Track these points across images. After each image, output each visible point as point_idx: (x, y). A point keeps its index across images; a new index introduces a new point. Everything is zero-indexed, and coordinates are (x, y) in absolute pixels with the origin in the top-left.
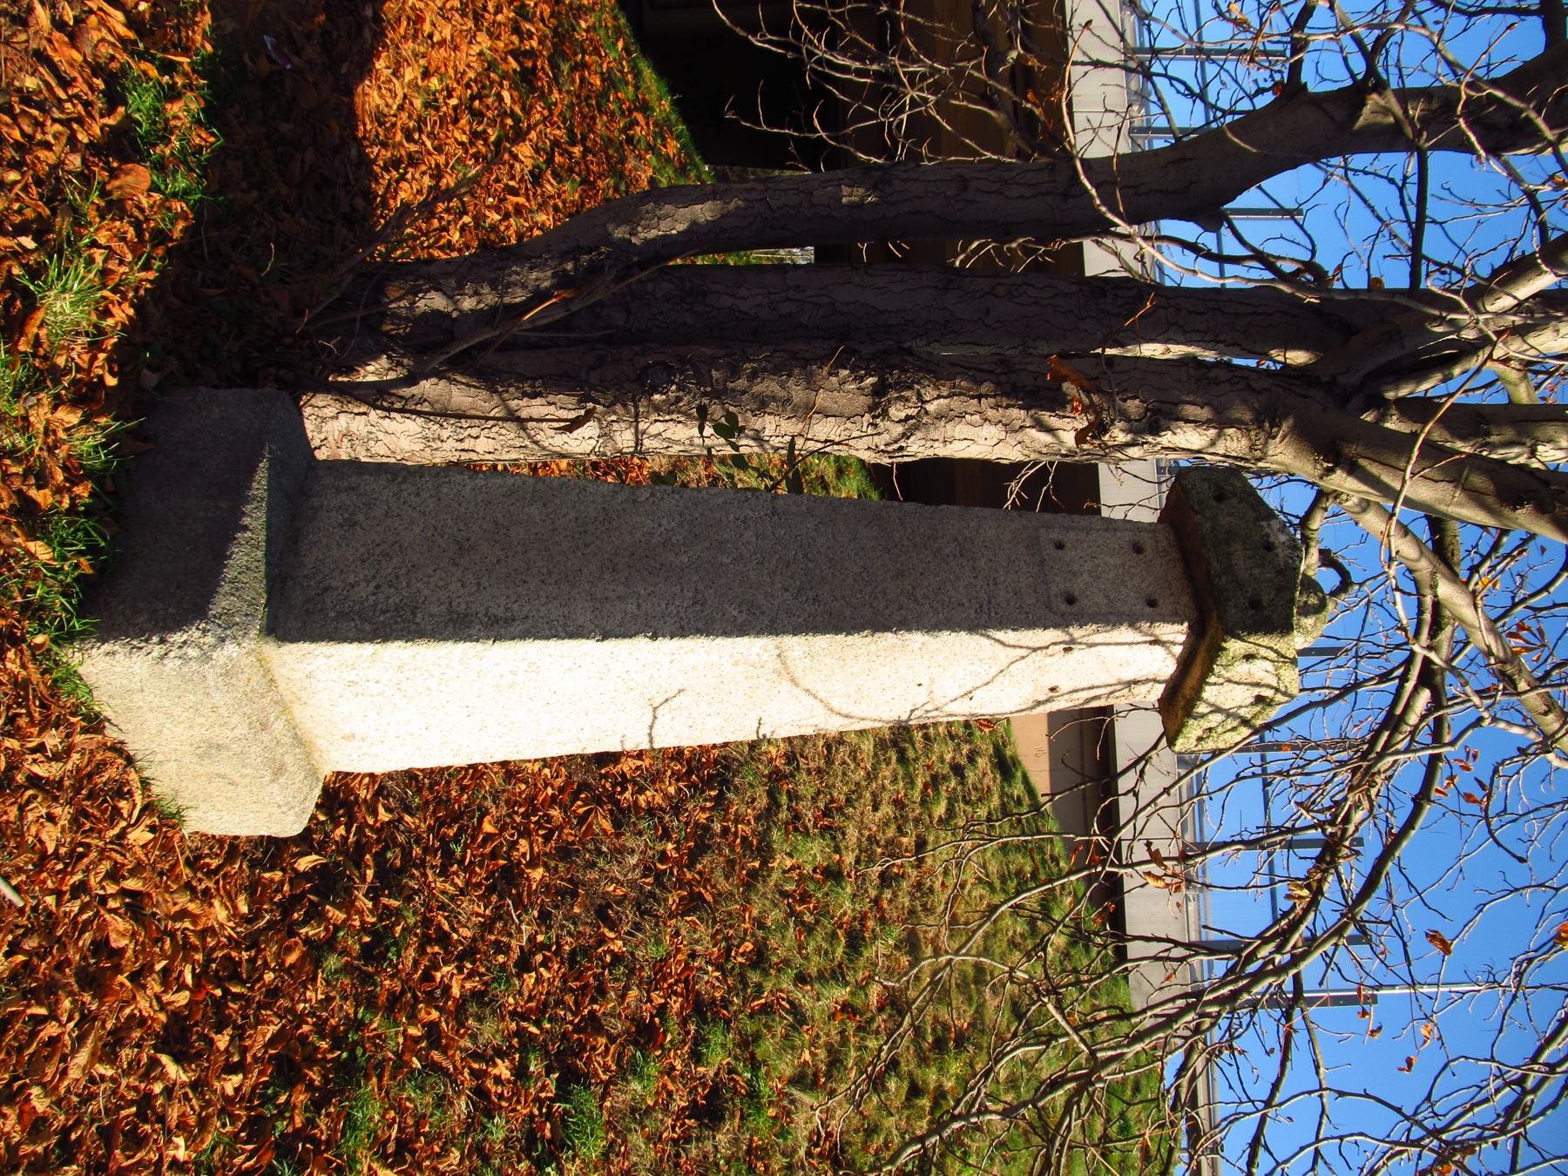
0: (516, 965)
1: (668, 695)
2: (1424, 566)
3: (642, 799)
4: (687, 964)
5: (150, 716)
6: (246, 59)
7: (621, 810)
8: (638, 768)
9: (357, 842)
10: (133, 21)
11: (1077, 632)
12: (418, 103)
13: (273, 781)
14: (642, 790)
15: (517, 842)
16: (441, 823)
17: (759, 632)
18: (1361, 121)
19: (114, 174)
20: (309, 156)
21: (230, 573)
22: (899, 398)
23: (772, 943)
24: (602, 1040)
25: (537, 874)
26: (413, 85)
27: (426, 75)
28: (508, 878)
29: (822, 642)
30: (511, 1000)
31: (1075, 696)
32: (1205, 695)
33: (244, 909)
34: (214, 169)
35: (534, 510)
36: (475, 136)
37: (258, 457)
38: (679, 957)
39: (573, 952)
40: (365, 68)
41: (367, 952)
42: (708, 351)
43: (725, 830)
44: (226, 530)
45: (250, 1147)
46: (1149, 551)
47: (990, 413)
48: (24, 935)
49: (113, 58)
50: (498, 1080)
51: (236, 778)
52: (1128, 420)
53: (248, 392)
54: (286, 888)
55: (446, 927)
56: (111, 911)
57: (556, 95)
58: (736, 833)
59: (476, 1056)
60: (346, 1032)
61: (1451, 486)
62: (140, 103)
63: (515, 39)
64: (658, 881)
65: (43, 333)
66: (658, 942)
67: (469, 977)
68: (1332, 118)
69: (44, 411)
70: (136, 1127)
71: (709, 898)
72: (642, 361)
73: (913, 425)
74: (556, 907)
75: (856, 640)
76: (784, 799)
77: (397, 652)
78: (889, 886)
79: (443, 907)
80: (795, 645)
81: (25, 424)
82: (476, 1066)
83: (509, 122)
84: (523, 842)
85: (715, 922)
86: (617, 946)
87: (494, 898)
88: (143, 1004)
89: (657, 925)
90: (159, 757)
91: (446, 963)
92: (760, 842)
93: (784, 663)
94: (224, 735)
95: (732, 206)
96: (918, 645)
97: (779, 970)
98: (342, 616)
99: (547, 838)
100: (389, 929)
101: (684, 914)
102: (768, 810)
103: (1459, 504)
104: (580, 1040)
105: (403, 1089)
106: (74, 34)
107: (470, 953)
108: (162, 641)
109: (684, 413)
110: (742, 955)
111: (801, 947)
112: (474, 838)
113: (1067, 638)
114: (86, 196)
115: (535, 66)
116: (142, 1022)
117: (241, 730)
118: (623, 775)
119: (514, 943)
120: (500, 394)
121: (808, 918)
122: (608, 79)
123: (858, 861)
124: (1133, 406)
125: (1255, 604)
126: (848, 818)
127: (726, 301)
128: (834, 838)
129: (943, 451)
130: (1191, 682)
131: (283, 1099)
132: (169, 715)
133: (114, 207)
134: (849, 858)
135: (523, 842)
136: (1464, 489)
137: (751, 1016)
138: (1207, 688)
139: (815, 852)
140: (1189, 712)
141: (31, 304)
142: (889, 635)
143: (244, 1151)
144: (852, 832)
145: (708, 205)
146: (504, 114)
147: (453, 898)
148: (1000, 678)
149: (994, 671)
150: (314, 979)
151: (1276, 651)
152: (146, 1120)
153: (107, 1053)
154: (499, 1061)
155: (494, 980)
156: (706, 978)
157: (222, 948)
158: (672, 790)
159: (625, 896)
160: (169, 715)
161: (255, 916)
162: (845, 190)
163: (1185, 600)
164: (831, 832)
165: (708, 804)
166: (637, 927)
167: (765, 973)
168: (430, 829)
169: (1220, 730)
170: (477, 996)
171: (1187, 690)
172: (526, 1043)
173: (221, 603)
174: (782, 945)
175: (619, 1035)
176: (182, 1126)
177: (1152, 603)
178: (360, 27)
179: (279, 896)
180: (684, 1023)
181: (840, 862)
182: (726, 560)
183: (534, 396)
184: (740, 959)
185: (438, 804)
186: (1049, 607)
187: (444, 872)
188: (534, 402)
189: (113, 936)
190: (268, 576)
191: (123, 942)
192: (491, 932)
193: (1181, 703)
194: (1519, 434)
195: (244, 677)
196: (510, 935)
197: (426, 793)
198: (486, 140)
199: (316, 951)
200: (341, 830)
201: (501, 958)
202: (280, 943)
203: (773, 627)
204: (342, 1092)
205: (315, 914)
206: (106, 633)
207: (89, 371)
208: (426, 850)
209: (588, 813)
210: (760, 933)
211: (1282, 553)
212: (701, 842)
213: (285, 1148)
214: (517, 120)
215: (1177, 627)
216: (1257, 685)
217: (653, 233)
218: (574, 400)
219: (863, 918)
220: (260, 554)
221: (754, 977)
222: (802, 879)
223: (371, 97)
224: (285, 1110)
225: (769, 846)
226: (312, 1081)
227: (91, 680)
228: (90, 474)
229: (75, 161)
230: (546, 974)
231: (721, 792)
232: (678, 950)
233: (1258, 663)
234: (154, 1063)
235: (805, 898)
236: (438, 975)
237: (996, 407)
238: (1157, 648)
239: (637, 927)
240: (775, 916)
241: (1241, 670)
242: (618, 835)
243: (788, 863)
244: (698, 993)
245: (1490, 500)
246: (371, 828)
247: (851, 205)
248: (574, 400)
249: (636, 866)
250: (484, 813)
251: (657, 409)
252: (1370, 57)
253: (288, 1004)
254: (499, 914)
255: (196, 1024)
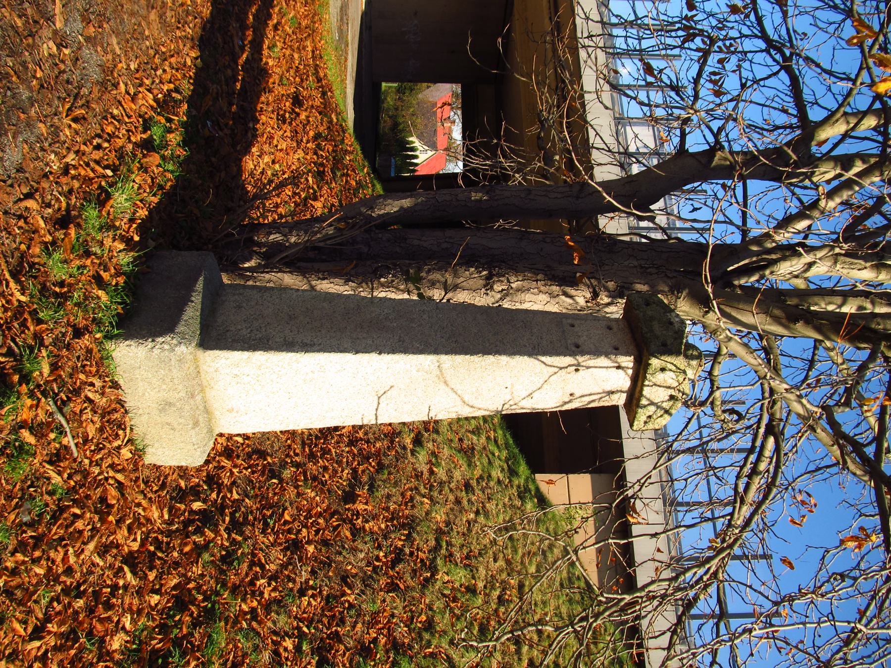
0: (298, 592)
1: (386, 389)
2: (764, 370)
3: (367, 525)
4: (389, 620)
5: (141, 384)
6: (200, 126)
7: (356, 529)
8: (366, 510)
9: (222, 504)
10: (156, 100)
11: (580, 359)
12: (269, 173)
13: (193, 428)
14: (367, 521)
15: (301, 530)
16: (264, 507)
17: (429, 353)
18: (714, 163)
19: (144, 156)
20: (223, 175)
21: (185, 317)
22: (499, 281)
23: (437, 618)
24: (342, 647)
25: (311, 549)
26: (267, 164)
27: (274, 162)
28: (295, 546)
29: (459, 359)
30: (295, 609)
31: (584, 399)
32: (644, 393)
33: (166, 517)
34: (184, 164)
35: (325, 305)
36: (295, 194)
37: (200, 275)
38: (385, 614)
39: (328, 596)
40: (247, 150)
41: (223, 559)
42: (407, 262)
43: (412, 554)
44: (185, 300)
45: (160, 637)
46: (615, 329)
47: (542, 288)
48: (74, 473)
49: (146, 113)
50: (286, 649)
51: (176, 426)
52: (609, 291)
53: (195, 253)
54: (186, 514)
55: (263, 561)
56: (109, 484)
57: (334, 185)
58: (417, 556)
59: (275, 633)
60: (211, 595)
61: (764, 316)
62: (156, 132)
63: (315, 157)
64: (375, 568)
65: (112, 210)
66: (374, 602)
67: (275, 589)
68: (700, 162)
69: (110, 240)
70: (109, 599)
71: (402, 586)
72: (376, 265)
73: (505, 294)
74: (320, 569)
75: (476, 359)
76: (444, 544)
77: (259, 357)
78: (504, 605)
79: (261, 549)
80: (447, 361)
81: (101, 244)
82: (275, 638)
83: (311, 191)
84: (304, 530)
85: (405, 600)
86: (351, 599)
87: (289, 553)
88: (119, 536)
89: (373, 593)
90: (141, 412)
91: (263, 578)
92: (430, 564)
93: (441, 371)
94: (173, 397)
95: (420, 200)
96: (505, 363)
97: (440, 636)
98: (234, 341)
99: (317, 532)
100: (235, 551)
101: (388, 592)
102: (435, 548)
103: (769, 324)
104: (330, 643)
105: (237, 635)
106: (134, 99)
107: (274, 577)
108: (153, 341)
109: (395, 288)
110: (420, 622)
111: (453, 625)
112: (279, 520)
113: (576, 362)
114: (133, 162)
115: (324, 170)
116: (118, 546)
117: (182, 394)
118: (358, 511)
119: (298, 579)
120: (307, 278)
121: (457, 611)
122: (359, 183)
123: (485, 587)
124: (611, 285)
125: (664, 345)
126: (479, 562)
127: (416, 242)
128: (472, 571)
129: (518, 306)
130: (638, 389)
131: (177, 618)
132: (150, 383)
133: (144, 169)
134: (481, 585)
135: (304, 530)
136: (771, 316)
137: (424, 657)
138: (645, 388)
139: (460, 576)
140: (638, 406)
141: (109, 196)
142: (491, 356)
143: (156, 639)
144: (482, 571)
145: (408, 200)
146: (309, 187)
147: (267, 547)
148: (545, 386)
149: (542, 381)
150: (197, 563)
151: (675, 366)
152: (114, 596)
153: (103, 551)
154: (287, 639)
155: (286, 595)
156: (400, 630)
157: (154, 532)
158: (383, 526)
159: (356, 574)
160: (150, 383)
161: (170, 523)
162: (473, 194)
163: (632, 347)
164: (471, 569)
165: (403, 538)
166: (363, 592)
167: (433, 635)
168: (257, 509)
169: (655, 417)
170: (278, 602)
171: (637, 395)
172: (301, 636)
173: (180, 328)
174: (443, 622)
175: (351, 648)
176: (130, 610)
177: (616, 349)
178: (247, 132)
179: (182, 518)
180: (387, 652)
181: (475, 585)
182: (414, 325)
183: (324, 279)
184: (419, 625)
185: (263, 497)
186: (567, 348)
187: (264, 532)
188: (323, 282)
189: (109, 497)
190: (201, 323)
191: (114, 502)
192: (286, 569)
193: (635, 402)
194: (801, 301)
195: (187, 365)
196: (296, 574)
197: (257, 490)
198: (300, 197)
199: (199, 550)
200: (214, 495)
201: (291, 585)
202: (182, 540)
203: (436, 351)
204: (208, 623)
205: (199, 531)
206: (127, 336)
207: (128, 232)
208: (255, 519)
209: (339, 525)
210: (430, 613)
211: (677, 326)
212: (398, 557)
213: (177, 642)
214: (315, 192)
215: (628, 358)
216: (669, 387)
217: (382, 212)
218: (343, 281)
219: (488, 619)
220: (198, 314)
221: (427, 636)
222: (453, 589)
223: (249, 164)
224: (178, 624)
225: (435, 567)
226: (193, 612)
227: (117, 361)
228: (124, 274)
229: (130, 147)
230: (314, 603)
231: (410, 534)
232: (385, 610)
233: (668, 372)
234: (121, 569)
235: (455, 600)
236: (258, 583)
237: (545, 285)
238: (620, 371)
239: (363, 592)
240: (438, 605)
241: (660, 378)
242: (354, 541)
243: (446, 578)
244: (395, 638)
245: (784, 321)
246: (229, 499)
247: (476, 201)
248: (343, 281)
249: (362, 560)
250: (285, 509)
251: (383, 285)
252: (716, 136)
253: (183, 571)
254: (289, 562)
255: (140, 563)
